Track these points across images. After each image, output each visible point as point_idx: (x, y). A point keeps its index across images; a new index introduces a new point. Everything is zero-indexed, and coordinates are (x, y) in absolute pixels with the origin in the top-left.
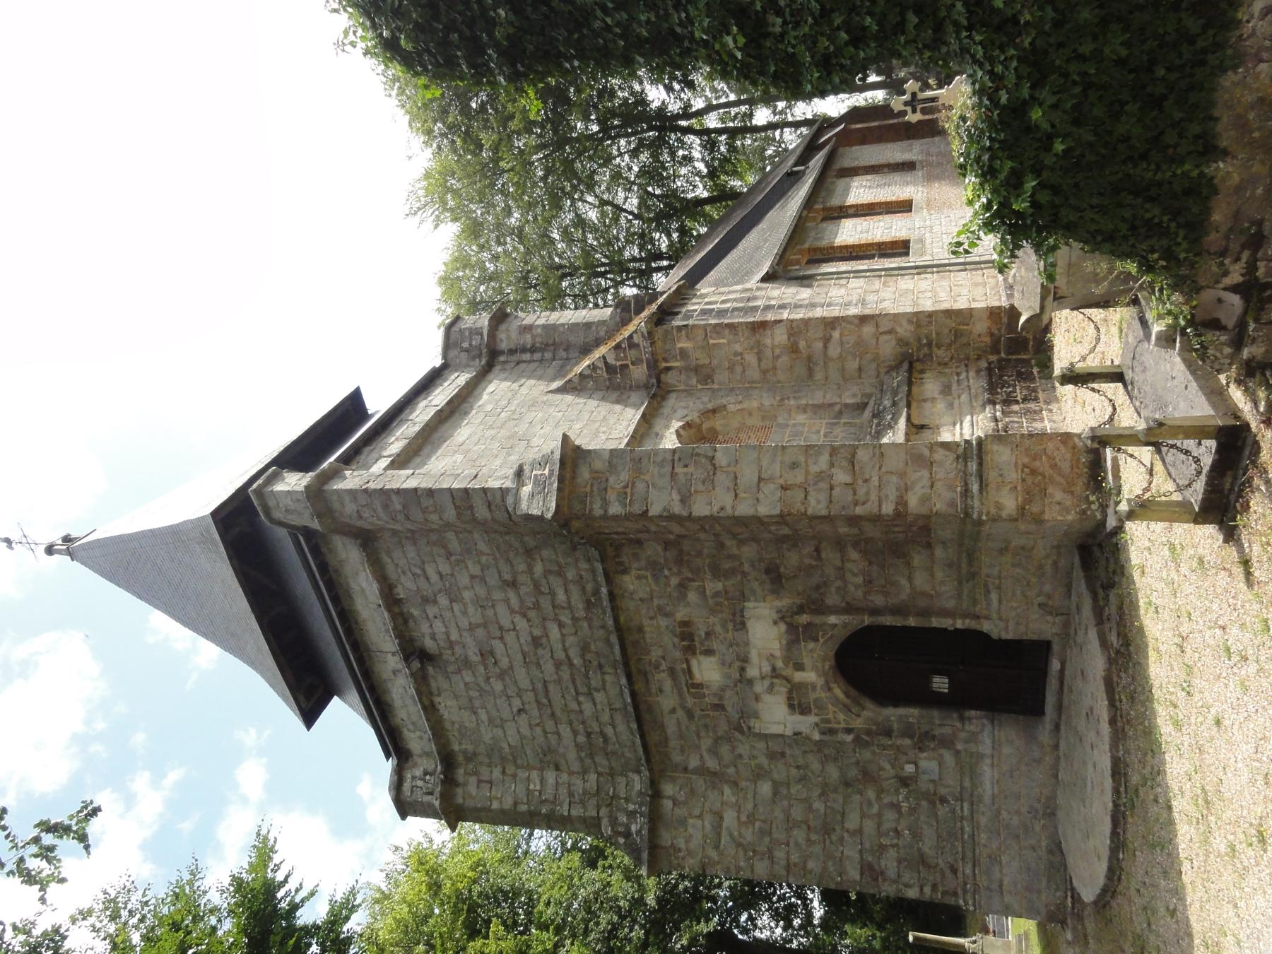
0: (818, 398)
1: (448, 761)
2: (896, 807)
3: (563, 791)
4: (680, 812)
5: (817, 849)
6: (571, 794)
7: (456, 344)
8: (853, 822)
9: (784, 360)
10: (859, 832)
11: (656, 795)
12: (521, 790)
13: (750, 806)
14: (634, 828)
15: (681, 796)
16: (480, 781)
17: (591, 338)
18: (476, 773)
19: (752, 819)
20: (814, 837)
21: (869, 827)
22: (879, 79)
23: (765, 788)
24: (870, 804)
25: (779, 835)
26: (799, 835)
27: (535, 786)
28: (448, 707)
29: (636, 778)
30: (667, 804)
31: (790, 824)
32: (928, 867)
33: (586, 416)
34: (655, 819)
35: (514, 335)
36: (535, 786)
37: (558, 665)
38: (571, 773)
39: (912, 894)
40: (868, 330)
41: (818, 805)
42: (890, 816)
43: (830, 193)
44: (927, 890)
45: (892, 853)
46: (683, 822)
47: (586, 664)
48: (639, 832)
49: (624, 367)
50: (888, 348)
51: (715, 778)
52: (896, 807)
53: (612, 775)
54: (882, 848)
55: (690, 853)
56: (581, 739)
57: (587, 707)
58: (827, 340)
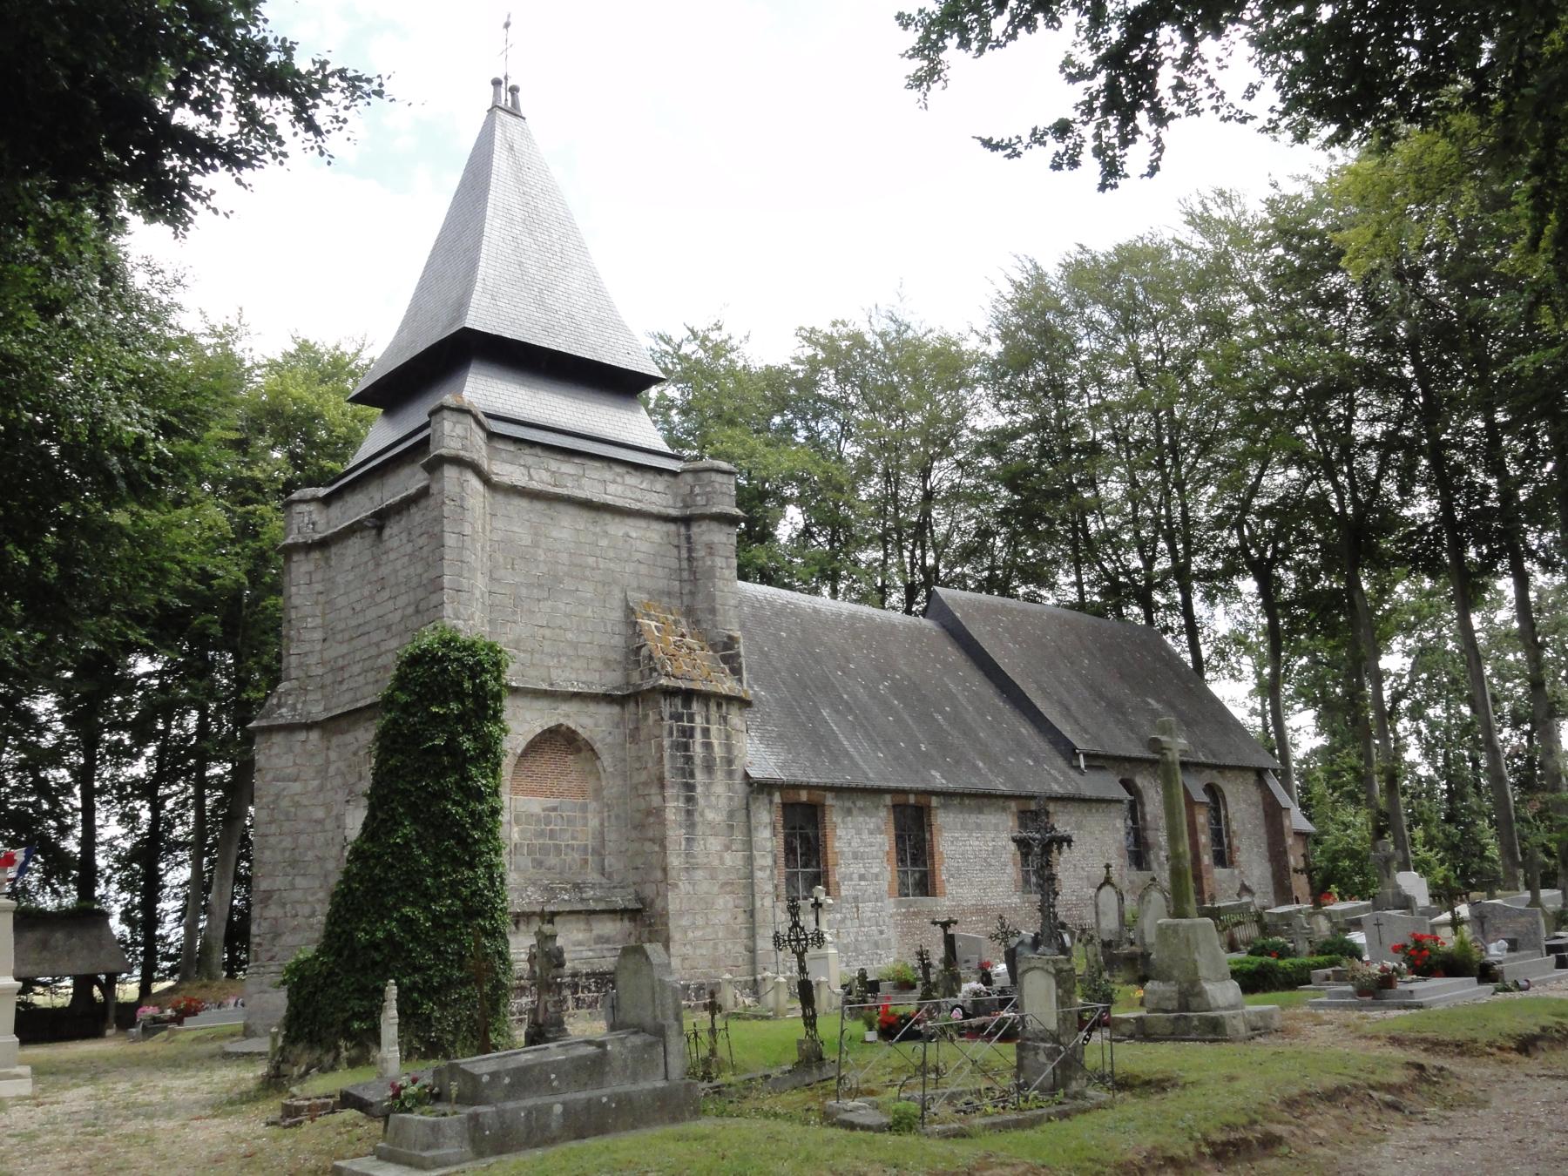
0: (611, 836)
1: (324, 544)
2: (313, 915)
4: (298, 748)
5: (279, 857)
6: (306, 654)
8: (301, 882)
9: (643, 805)
10: (294, 888)
11: (308, 727)
12: (307, 610)
14: (284, 710)
15: (309, 747)
16: (310, 573)
17: (700, 615)
18: (317, 567)
19: (297, 805)
20: (287, 854)
21: (297, 895)
23: (319, 813)
25: (287, 826)
26: (287, 842)
27: (310, 623)
29: (321, 708)
32: (274, 939)
33: (584, 639)
35: (706, 538)
36: (310, 623)
38: (321, 651)
39: (254, 929)
40: (659, 875)
41: (310, 855)
42: (306, 910)
43: (945, 807)
44: (257, 940)
45: (280, 913)
48: (281, 716)
49: (638, 662)
50: (649, 891)
51: (322, 772)
52: (313, 915)
53: (323, 687)
54: (284, 905)
55: (269, 758)
56: (341, 662)
58: (653, 840)
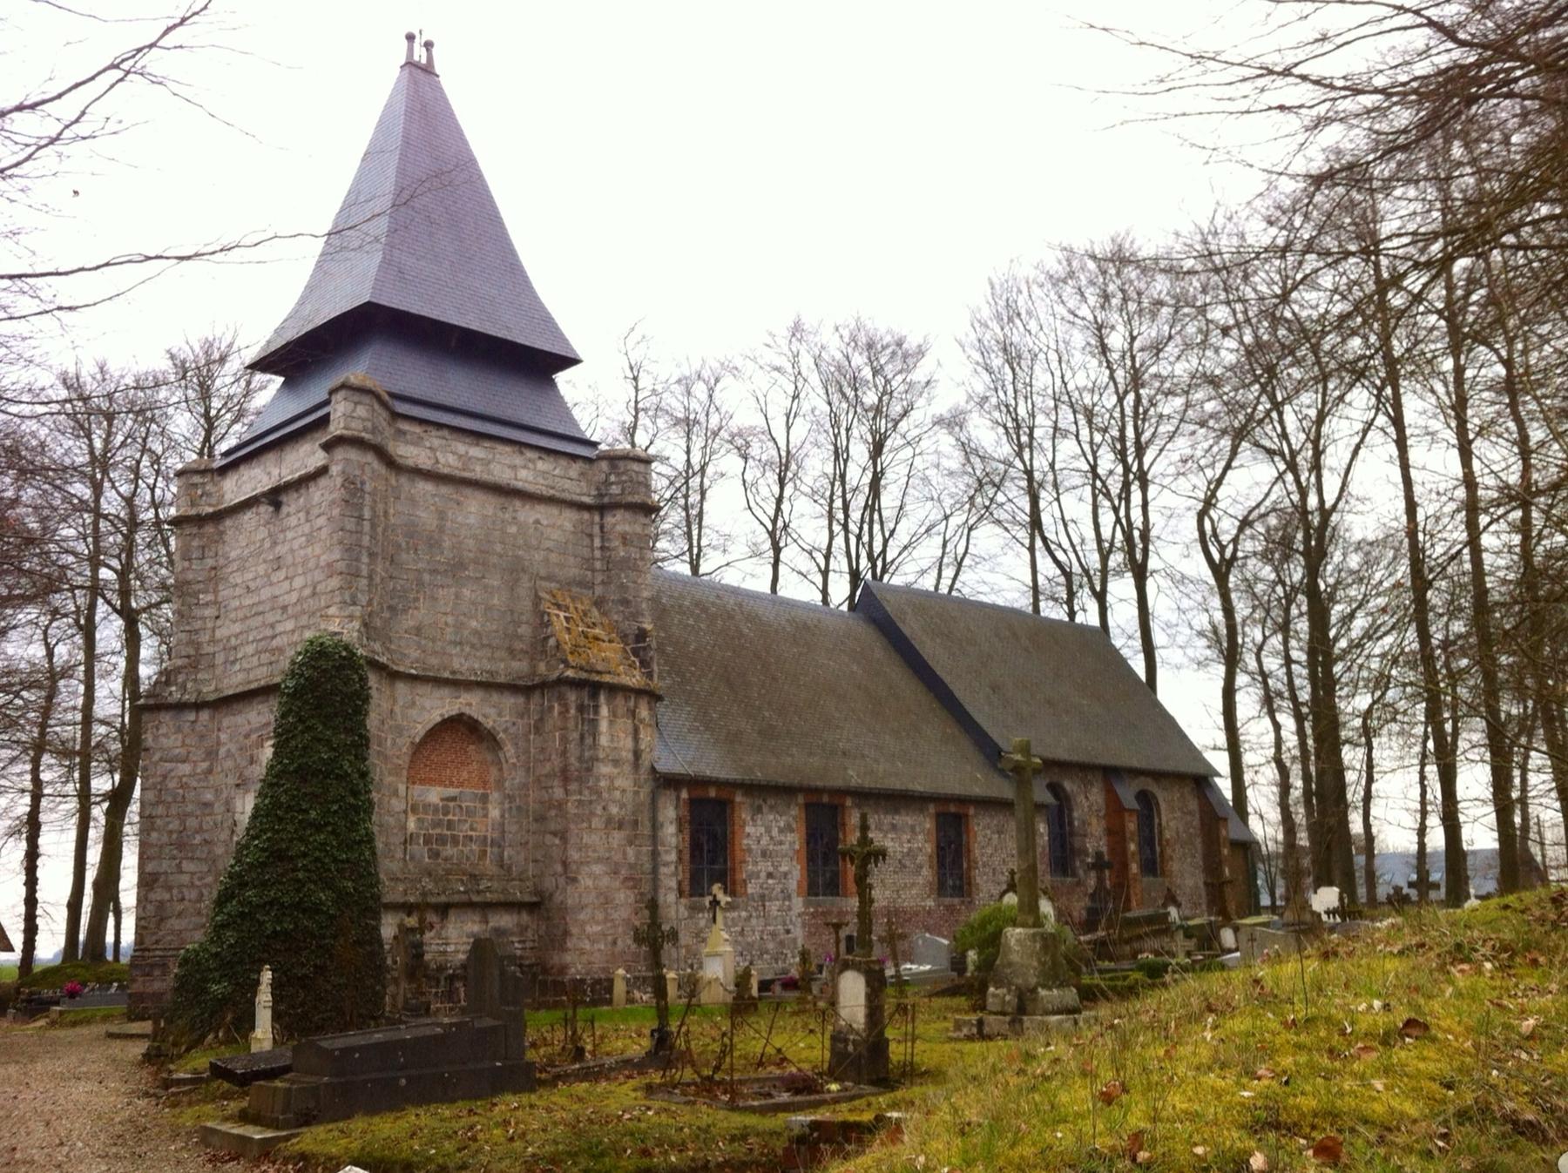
3: (198, 625)
5: (165, 839)
7: (613, 467)
8: (187, 866)
13: (194, 784)
15: (199, 727)
20: (174, 836)
21: (185, 878)
22: (1518, 812)
24: (201, 879)
26: (175, 825)
28: (248, 517)
30: (192, 717)
31: (183, 817)
34: (181, 707)
37: (272, 626)
42: (194, 895)
46: (179, 730)
47: (272, 651)
52: (200, 899)
56: (233, 641)
57: (250, 649)
58: (555, 834)
